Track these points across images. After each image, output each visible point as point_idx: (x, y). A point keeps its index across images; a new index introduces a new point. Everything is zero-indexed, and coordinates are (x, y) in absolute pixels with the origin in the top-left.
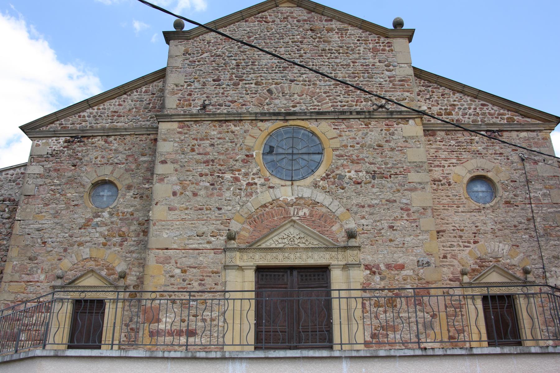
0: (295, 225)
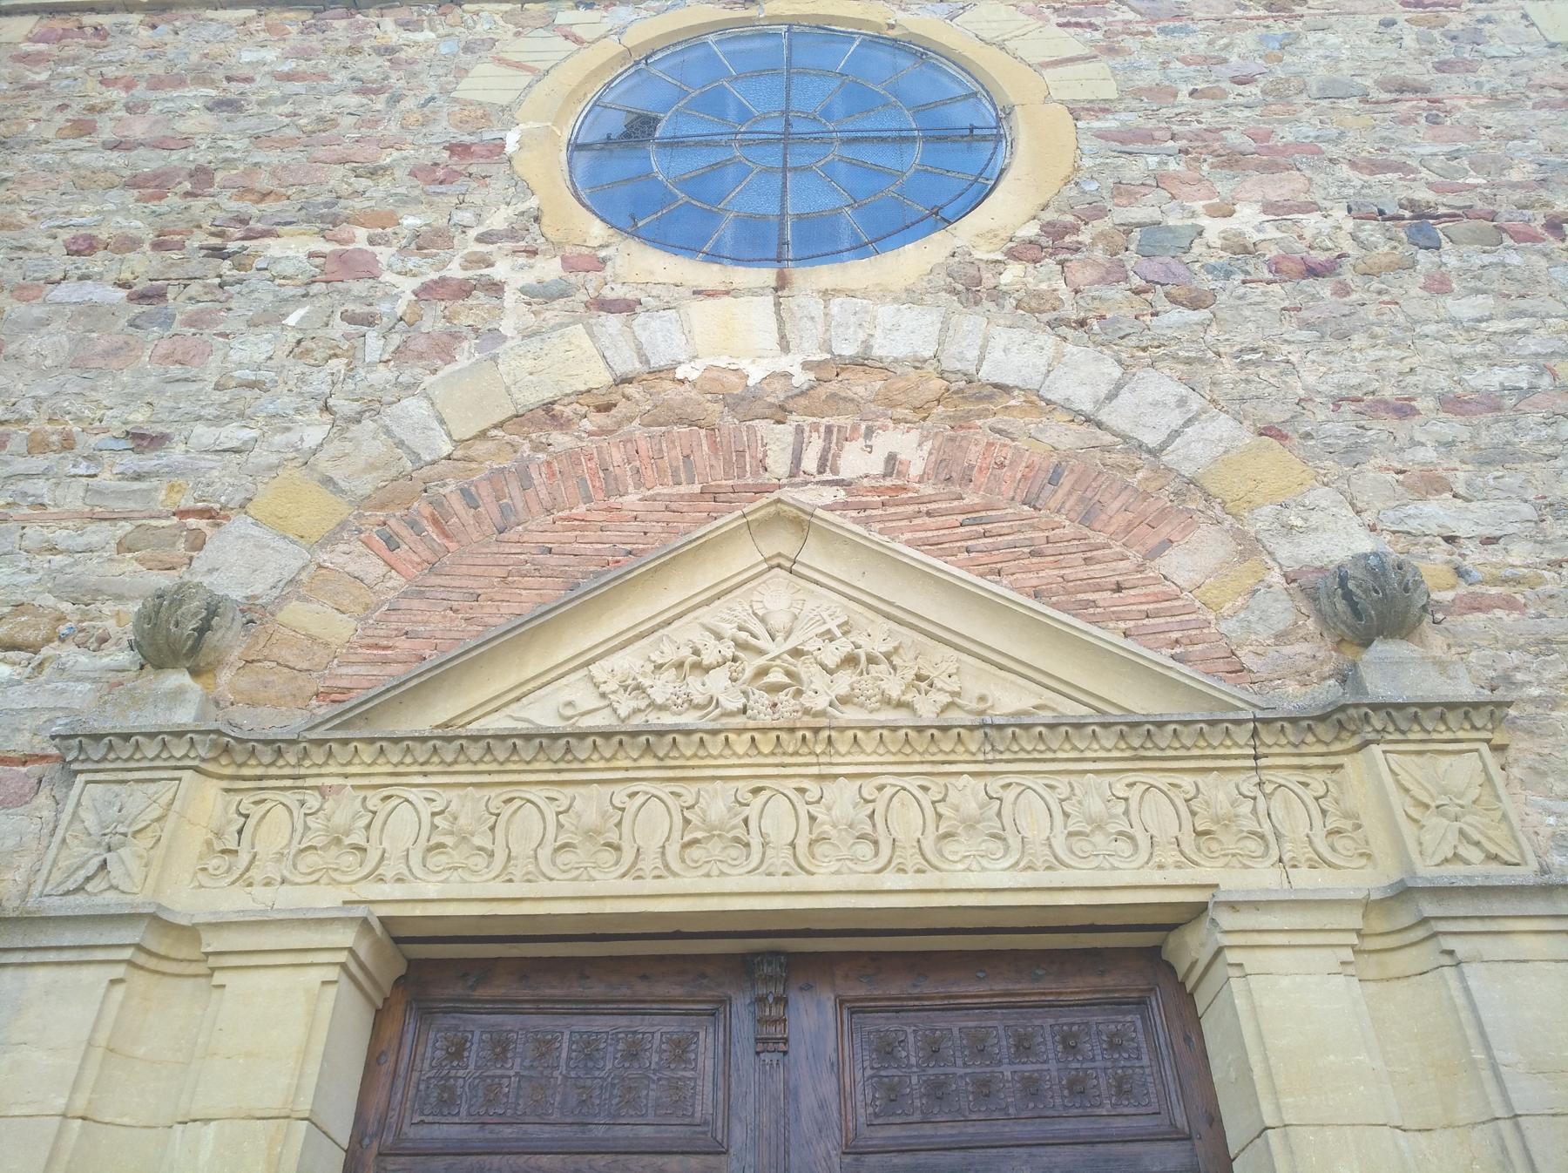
0: (813, 556)
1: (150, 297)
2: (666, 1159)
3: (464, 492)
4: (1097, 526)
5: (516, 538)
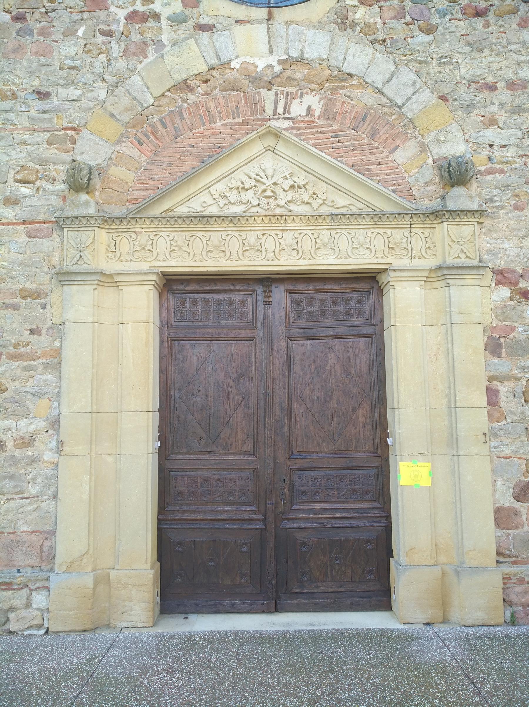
0: (281, 147)
1: (20, 19)
2: (241, 330)
3: (161, 121)
4: (376, 140)
5: (181, 141)
